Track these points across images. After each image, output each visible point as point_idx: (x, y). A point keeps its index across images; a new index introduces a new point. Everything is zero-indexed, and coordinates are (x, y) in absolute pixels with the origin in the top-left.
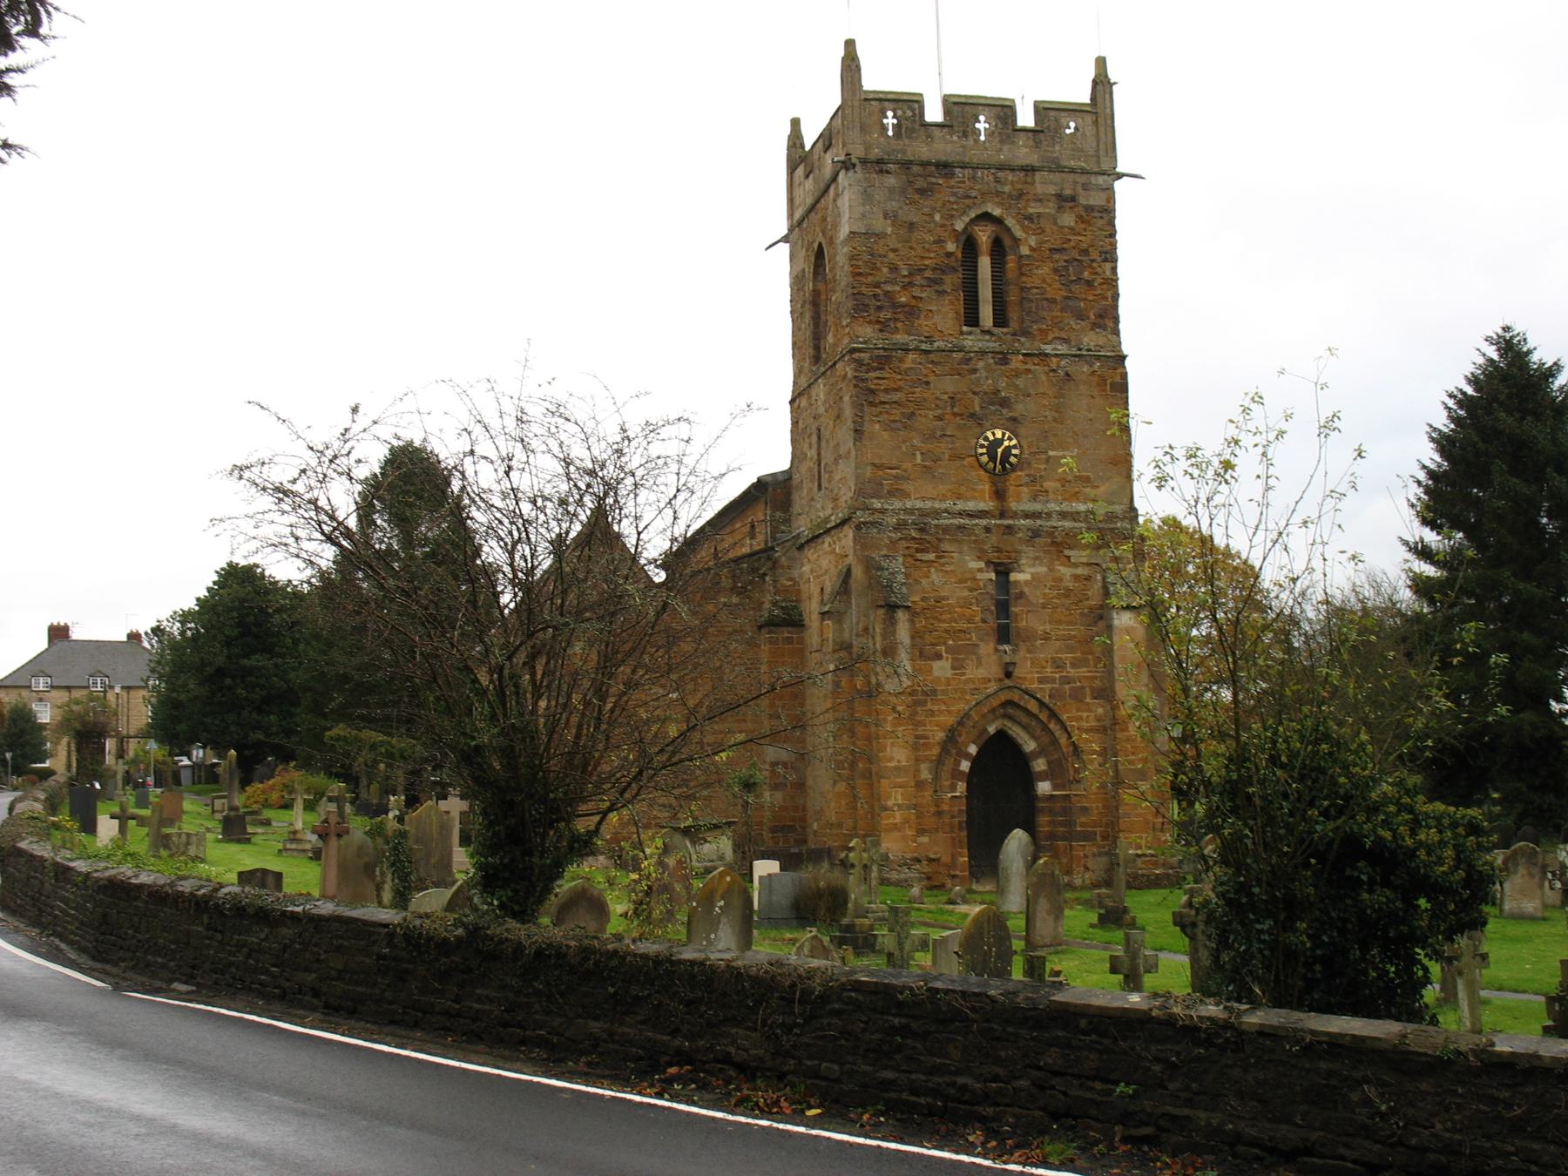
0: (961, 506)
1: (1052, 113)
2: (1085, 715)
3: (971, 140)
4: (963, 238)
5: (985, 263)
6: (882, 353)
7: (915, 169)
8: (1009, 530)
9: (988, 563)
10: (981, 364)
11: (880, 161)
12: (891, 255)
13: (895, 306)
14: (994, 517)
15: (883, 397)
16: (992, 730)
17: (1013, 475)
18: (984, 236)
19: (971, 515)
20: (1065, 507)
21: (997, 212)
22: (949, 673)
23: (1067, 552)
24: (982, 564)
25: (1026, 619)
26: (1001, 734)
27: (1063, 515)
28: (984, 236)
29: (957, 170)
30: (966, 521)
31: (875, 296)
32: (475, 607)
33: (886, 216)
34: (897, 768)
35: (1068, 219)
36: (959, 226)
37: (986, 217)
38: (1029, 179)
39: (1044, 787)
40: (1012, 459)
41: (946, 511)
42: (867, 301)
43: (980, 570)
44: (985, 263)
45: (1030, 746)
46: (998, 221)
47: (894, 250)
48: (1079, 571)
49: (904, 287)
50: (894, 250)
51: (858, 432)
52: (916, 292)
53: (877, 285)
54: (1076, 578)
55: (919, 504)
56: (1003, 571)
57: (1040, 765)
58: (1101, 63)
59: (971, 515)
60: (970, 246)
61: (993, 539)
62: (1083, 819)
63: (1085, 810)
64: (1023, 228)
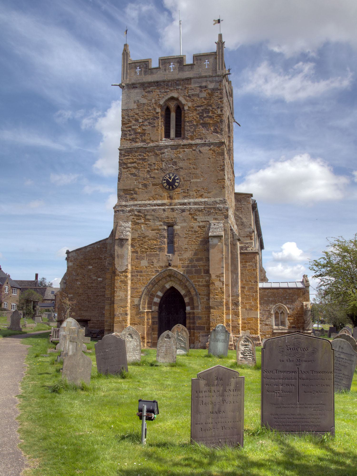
0: (155, 202)
1: (199, 57)
2: (201, 280)
3: (167, 71)
4: (165, 107)
5: (173, 115)
6: (129, 150)
7: (146, 85)
8: (173, 210)
9: (164, 222)
10: (166, 150)
11: (133, 84)
12: (136, 116)
13: (136, 133)
14: (168, 206)
15: (129, 165)
16: (168, 286)
17: (176, 190)
18: (172, 105)
19: (158, 205)
20: (197, 200)
21: (175, 95)
22: (147, 265)
23: (195, 217)
24: (162, 223)
25: (180, 242)
26: (172, 288)
27: (195, 203)
28: (172, 105)
29: (162, 83)
30: (157, 207)
31: (129, 131)
32: (291, 308)
33: (135, 102)
34: (121, 300)
35: (204, 95)
36: (162, 102)
37: (172, 98)
38: (189, 82)
39: (188, 309)
40: (176, 184)
41: (149, 204)
42: (126, 133)
43: (161, 225)
44: (173, 115)
45: (183, 292)
46: (177, 99)
47: (137, 114)
48: (201, 224)
49: (140, 127)
50: (137, 114)
51: (332, 252)
52: (144, 128)
53: (130, 127)
54: (199, 227)
55: (139, 202)
56: (170, 226)
57: (186, 300)
58: (220, 36)
59: (158, 205)
60: (168, 111)
61: (166, 214)
62: (199, 321)
63: (200, 318)
64: (187, 101)
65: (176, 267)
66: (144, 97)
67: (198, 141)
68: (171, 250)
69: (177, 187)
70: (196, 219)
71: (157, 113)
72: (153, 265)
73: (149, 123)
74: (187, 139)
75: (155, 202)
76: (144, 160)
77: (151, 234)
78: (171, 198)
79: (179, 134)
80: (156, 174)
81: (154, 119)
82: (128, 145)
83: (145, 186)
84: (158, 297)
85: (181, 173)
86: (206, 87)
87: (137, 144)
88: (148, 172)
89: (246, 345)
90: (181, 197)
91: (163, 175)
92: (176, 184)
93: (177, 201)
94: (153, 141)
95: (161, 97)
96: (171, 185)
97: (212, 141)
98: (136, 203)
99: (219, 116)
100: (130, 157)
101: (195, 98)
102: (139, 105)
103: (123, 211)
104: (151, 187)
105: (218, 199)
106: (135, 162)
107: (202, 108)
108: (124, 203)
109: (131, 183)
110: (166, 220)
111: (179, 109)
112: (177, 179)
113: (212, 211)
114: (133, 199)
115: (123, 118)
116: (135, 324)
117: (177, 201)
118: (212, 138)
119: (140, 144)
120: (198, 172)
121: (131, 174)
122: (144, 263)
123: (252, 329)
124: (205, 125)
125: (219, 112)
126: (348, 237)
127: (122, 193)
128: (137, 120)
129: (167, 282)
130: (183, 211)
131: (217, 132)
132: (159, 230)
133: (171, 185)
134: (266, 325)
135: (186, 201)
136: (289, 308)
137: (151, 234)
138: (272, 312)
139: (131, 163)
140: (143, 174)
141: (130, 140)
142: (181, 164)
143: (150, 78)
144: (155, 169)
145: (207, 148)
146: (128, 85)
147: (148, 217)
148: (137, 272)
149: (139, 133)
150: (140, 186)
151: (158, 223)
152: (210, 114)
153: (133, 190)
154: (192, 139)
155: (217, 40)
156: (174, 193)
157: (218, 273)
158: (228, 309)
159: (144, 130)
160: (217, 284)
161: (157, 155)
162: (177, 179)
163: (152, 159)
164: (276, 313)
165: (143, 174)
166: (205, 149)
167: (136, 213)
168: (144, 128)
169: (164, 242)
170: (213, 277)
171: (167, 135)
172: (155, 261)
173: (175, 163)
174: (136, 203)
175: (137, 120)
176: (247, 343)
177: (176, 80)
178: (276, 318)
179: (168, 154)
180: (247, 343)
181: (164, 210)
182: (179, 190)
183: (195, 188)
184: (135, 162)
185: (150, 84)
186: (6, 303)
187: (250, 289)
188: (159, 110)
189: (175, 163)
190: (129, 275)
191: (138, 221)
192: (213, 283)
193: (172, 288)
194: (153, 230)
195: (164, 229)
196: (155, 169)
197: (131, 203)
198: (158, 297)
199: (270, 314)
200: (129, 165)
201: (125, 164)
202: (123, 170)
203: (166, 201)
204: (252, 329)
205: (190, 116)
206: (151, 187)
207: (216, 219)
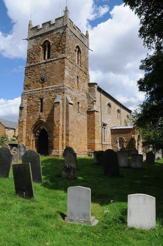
0: (37, 89)
18: (47, 44)
19: (38, 91)
20: (52, 86)
21: (47, 39)
23: (51, 94)
25: (45, 107)
27: (52, 88)
44: (47, 48)
45: (47, 131)
47: (33, 51)
50: (33, 51)
52: (35, 56)
54: (53, 99)
55: (31, 90)
56: (42, 100)
64: (52, 41)
65: (43, 118)
66: (36, 42)
67: (55, 59)
68: (42, 111)
69: (45, 81)
70: (51, 95)
71: (40, 49)
72: (34, 118)
73: (37, 54)
74: (51, 58)
75: (36, 90)
76: (33, 71)
77: (34, 104)
78: (43, 87)
79: (49, 57)
80: (38, 76)
81: (39, 52)
82: (28, 65)
83: (33, 82)
84: (38, 133)
85: (47, 75)
86: (59, 33)
87: (32, 64)
88: (35, 76)
89: (14, 153)
90: (46, 86)
91: (40, 76)
92: (45, 80)
93: (45, 88)
94: (38, 62)
95: (41, 41)
96: (43, 81)
97: (60, 57)
98: (30, 90)
99: (64, 45)
100: (29, 70)
101: (55, 39)
102: (33, 46)
103: (24, 95)
104: (35, 82)
105: (61, 85)
106: (30, 72)
107: (57, 43)
108: (25, 91)
109: (29, 82)
110: (40, 97)
111: (49, 46)
112: (45, 78)
113: (58, 90)
114: (29, 89)
115: (28, 53)
116: (27, 146)
117: (45, 88)
118: (60, 56)
119: (33, 64)
120: (54, 73)
121: (29, 78)
122: (31, 118)
123: (92, 148)
124: (58, 50)
125: (64, 44)
126: (2, 101)
127: (25, 87)
128: (32, 54)
129: (41, 126)
130: (47, 92)
131: (63, 53)
132: (37, 102)
133: (43, 81)
134: (115, 147)
135: (48, 87)
136: (125, 139)
137: (34, 104)
138: (117, 141)
139: (29, 73)
140: (33, 77)
141: (29, 63)
142: (47, 71)
143: (38, 33)
144: (37, 74)
145: (58, 61)
146: (29, 38)
147: (34, 96)
148: (28, 122)
149: (33, 59)
150: (32, 83)
151: (37, 99)
152: (61, 45)
153: (29, 85)
154: (53, 58)
155: (64, 10)
156: (44, 84)
157: (57, 120)
158: (63, 137)
159: (35, 57)
160: (57, 125)
161: (38, 68)
162: (45, 78)
163: (37, 70)
164: (120, 141)
165: (33, 77)
166: (57, 62)
167: (29, 95)
168: (35, 56)
169: (39, 107)
170: (55, 122)
171: (44, 59)
172: (35, 116)
173: (45, 70)
174: (30, 90)
175: (32, 54)
176: (15, 152)
177: (47, 32)
178: (120, 143)
179: (43, 66)
180: (15, 152)
181: (39, 93)
182: (46, 83)
183: (52, 81)
184: (30, 72)
185: (38, 36)
186: (10, 137)
187: (91, 129)
188: (41, 47)
189: (45, 70)
190: (25, 123)
191: (29, 99)
192: (55, 125)
193: (44, 129)
194: (35, 102)
195: (39, 101)
196: (37, 74)
197: (28, 91)
198: (38, 133)
199: (117, 142)
200: (28, 74)
201: (27, 74)
202: (26, 77)
203: (41, 88)
204: (92, 148)
205: (53, 47)
206: (35, 82)
207: (59, 94)
